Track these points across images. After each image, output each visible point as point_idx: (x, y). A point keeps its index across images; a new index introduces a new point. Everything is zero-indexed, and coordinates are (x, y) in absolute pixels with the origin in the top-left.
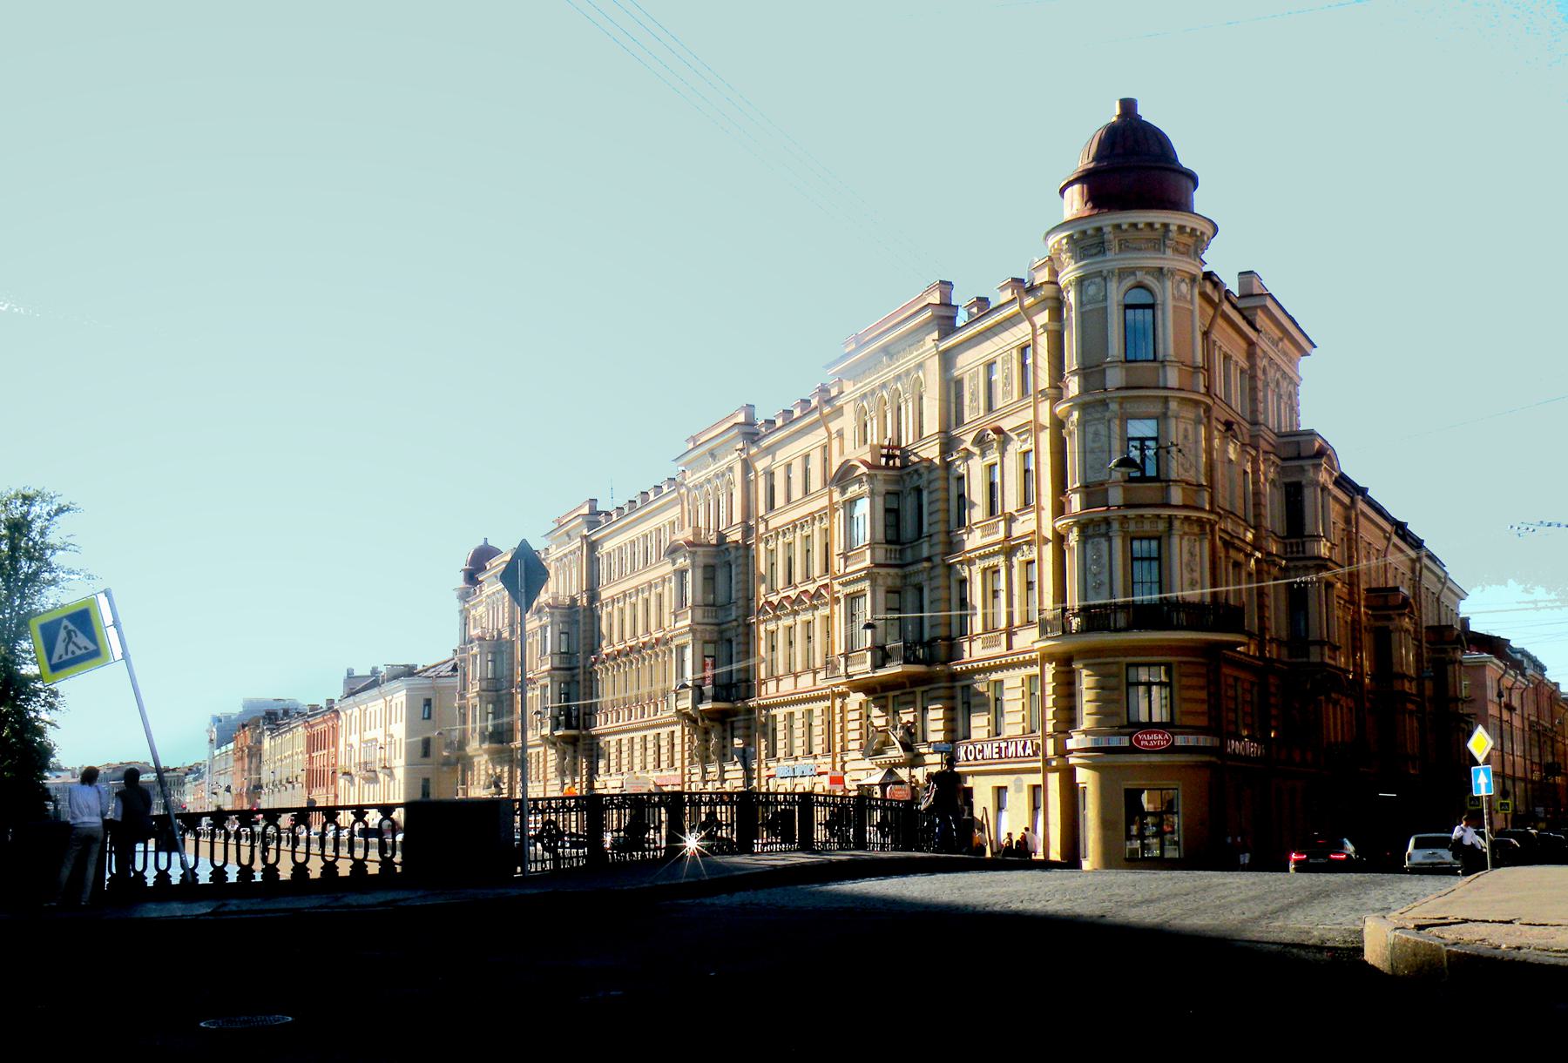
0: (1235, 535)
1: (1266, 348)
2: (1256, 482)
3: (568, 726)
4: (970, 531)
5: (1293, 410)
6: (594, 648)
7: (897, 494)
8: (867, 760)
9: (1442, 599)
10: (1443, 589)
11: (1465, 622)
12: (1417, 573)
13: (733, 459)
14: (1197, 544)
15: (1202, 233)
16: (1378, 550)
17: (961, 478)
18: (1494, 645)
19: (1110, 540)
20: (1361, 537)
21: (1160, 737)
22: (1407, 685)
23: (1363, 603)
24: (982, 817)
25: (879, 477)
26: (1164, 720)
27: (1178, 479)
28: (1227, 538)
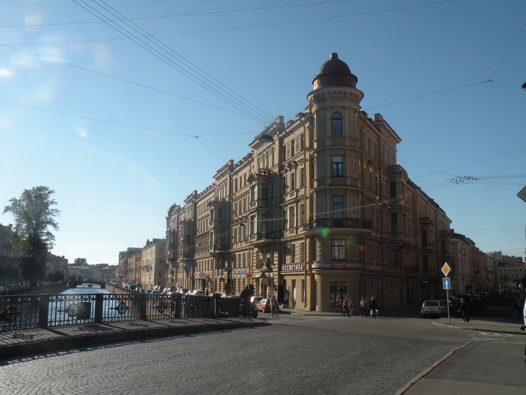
0: (371, 197)
1: (383, 138)
2: (380, 181)
3: (187, 257)
4: (287, 195)
5: (394, 159)
6: (195, 234)
7: (266, 184)
8: (257, 270)
9: (444, 222)
10: (427, 205)
11: (453, 230)
12: (436, 214)
13: (227, 176)
14: (356, 198)
15: (358, 95)
16: (423, 206)
17: (284, 178)
18: (461, 237)
19: (326, 197)
20: (418, 202)
21: (342, 264)
22: (432, 248)
23: (418, 222)
24: (288, 290)
25: (260, 179)
26: (344, 258)
27: (349, 176)
28: (369, 198)
